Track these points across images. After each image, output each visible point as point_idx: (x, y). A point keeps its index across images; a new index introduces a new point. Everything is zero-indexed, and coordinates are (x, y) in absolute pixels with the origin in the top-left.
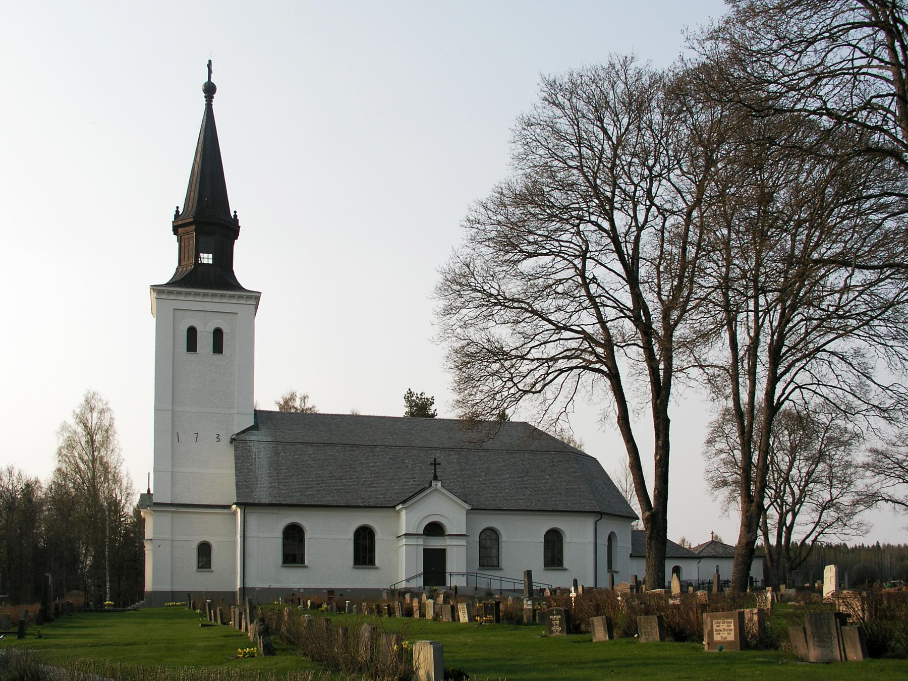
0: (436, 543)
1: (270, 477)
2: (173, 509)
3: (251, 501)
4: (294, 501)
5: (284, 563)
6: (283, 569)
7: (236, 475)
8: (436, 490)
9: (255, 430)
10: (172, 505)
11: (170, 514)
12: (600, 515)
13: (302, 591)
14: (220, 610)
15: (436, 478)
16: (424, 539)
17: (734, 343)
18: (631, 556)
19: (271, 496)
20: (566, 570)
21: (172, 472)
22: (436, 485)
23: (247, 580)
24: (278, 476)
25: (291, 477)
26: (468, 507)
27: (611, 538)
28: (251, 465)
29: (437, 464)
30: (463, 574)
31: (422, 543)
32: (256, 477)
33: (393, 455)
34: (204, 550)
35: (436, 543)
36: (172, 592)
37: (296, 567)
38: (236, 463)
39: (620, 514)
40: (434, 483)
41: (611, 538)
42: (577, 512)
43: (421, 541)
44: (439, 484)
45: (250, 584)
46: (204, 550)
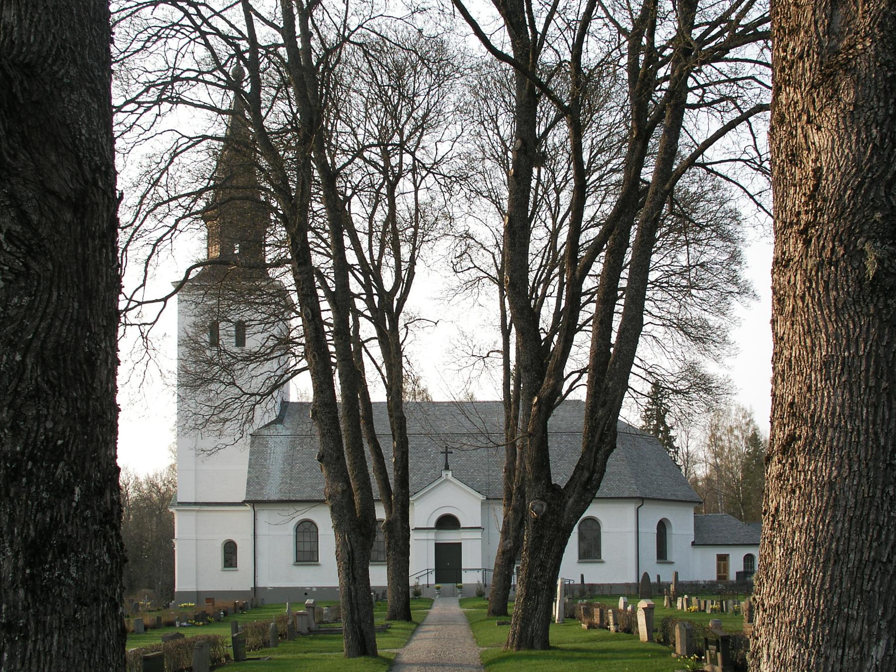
0: (449, 537)
1: (283, 472)
2: (197, 508)
3: (260, 498)
4: (304, 497)
5: (580, 558)
6: (295, 567)
7: (249, 472)
8: (447, 480)
9: (279, 423)
10: (196, 504)
11: (194, 514)
12: (642, 500)
13: (314, 589)
14: (648, 611)
15: (447, 468)
16: (435, 533)
17: (394, 322)
18: (693, 544)
19: (281, 492)
20: (603, 562)
21: (196, 470)
22: (447, 475)
23: (258, 579)
24: (291, 471)
25: (304, 471)
26: (481, 497)
27: (662, 527)
28: (266, 460)
29: (446, 450)
30: (478, 570)
31: (434, 538)
32: (268, 473)
33: (416, 444)
34: (230, 552)
35: (449, 537)
36: (198, 592)
37: (591, 562)
38: (250, 459)
39: (674, 498)
40: (444, 473)
41: (662, 527)
42: (605, 498)
43: (432, 535)
44: (450, 473)
45: (260, 584)
46: (230, 552)
